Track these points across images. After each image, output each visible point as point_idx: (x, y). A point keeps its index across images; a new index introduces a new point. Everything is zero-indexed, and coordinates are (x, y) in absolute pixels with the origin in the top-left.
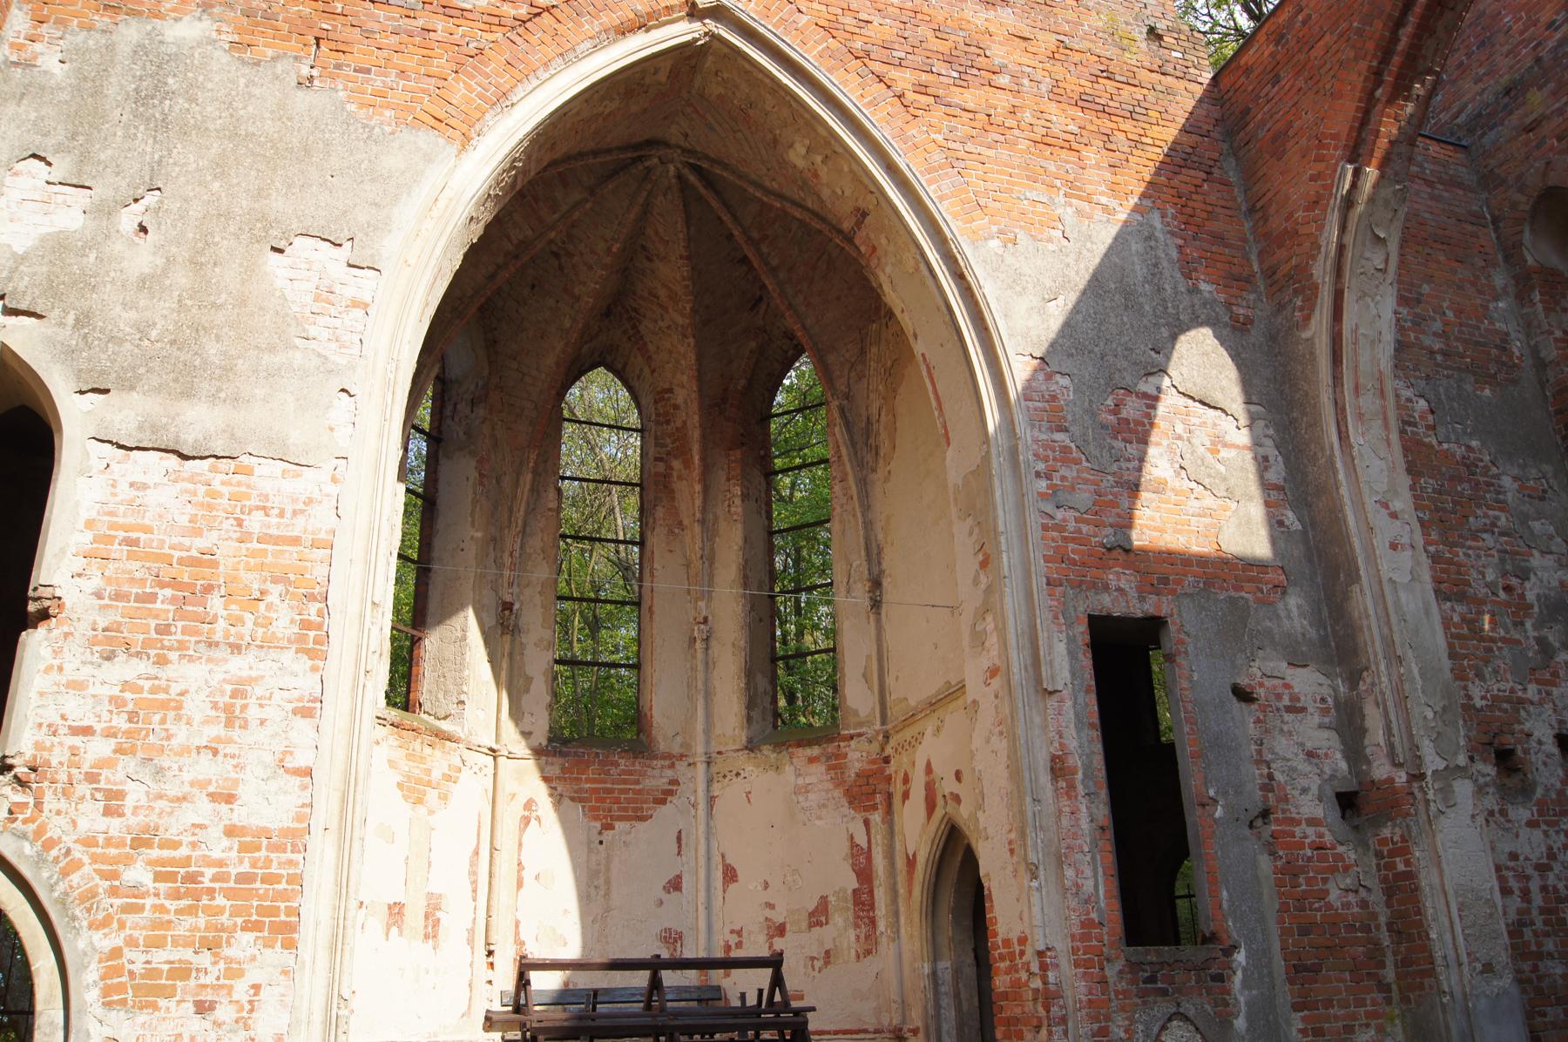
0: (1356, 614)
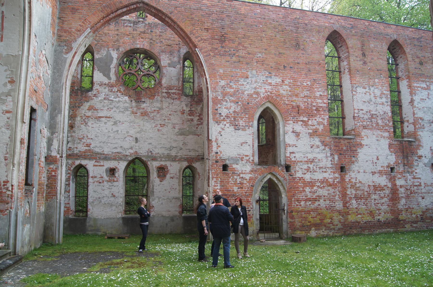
0: (58, 120)
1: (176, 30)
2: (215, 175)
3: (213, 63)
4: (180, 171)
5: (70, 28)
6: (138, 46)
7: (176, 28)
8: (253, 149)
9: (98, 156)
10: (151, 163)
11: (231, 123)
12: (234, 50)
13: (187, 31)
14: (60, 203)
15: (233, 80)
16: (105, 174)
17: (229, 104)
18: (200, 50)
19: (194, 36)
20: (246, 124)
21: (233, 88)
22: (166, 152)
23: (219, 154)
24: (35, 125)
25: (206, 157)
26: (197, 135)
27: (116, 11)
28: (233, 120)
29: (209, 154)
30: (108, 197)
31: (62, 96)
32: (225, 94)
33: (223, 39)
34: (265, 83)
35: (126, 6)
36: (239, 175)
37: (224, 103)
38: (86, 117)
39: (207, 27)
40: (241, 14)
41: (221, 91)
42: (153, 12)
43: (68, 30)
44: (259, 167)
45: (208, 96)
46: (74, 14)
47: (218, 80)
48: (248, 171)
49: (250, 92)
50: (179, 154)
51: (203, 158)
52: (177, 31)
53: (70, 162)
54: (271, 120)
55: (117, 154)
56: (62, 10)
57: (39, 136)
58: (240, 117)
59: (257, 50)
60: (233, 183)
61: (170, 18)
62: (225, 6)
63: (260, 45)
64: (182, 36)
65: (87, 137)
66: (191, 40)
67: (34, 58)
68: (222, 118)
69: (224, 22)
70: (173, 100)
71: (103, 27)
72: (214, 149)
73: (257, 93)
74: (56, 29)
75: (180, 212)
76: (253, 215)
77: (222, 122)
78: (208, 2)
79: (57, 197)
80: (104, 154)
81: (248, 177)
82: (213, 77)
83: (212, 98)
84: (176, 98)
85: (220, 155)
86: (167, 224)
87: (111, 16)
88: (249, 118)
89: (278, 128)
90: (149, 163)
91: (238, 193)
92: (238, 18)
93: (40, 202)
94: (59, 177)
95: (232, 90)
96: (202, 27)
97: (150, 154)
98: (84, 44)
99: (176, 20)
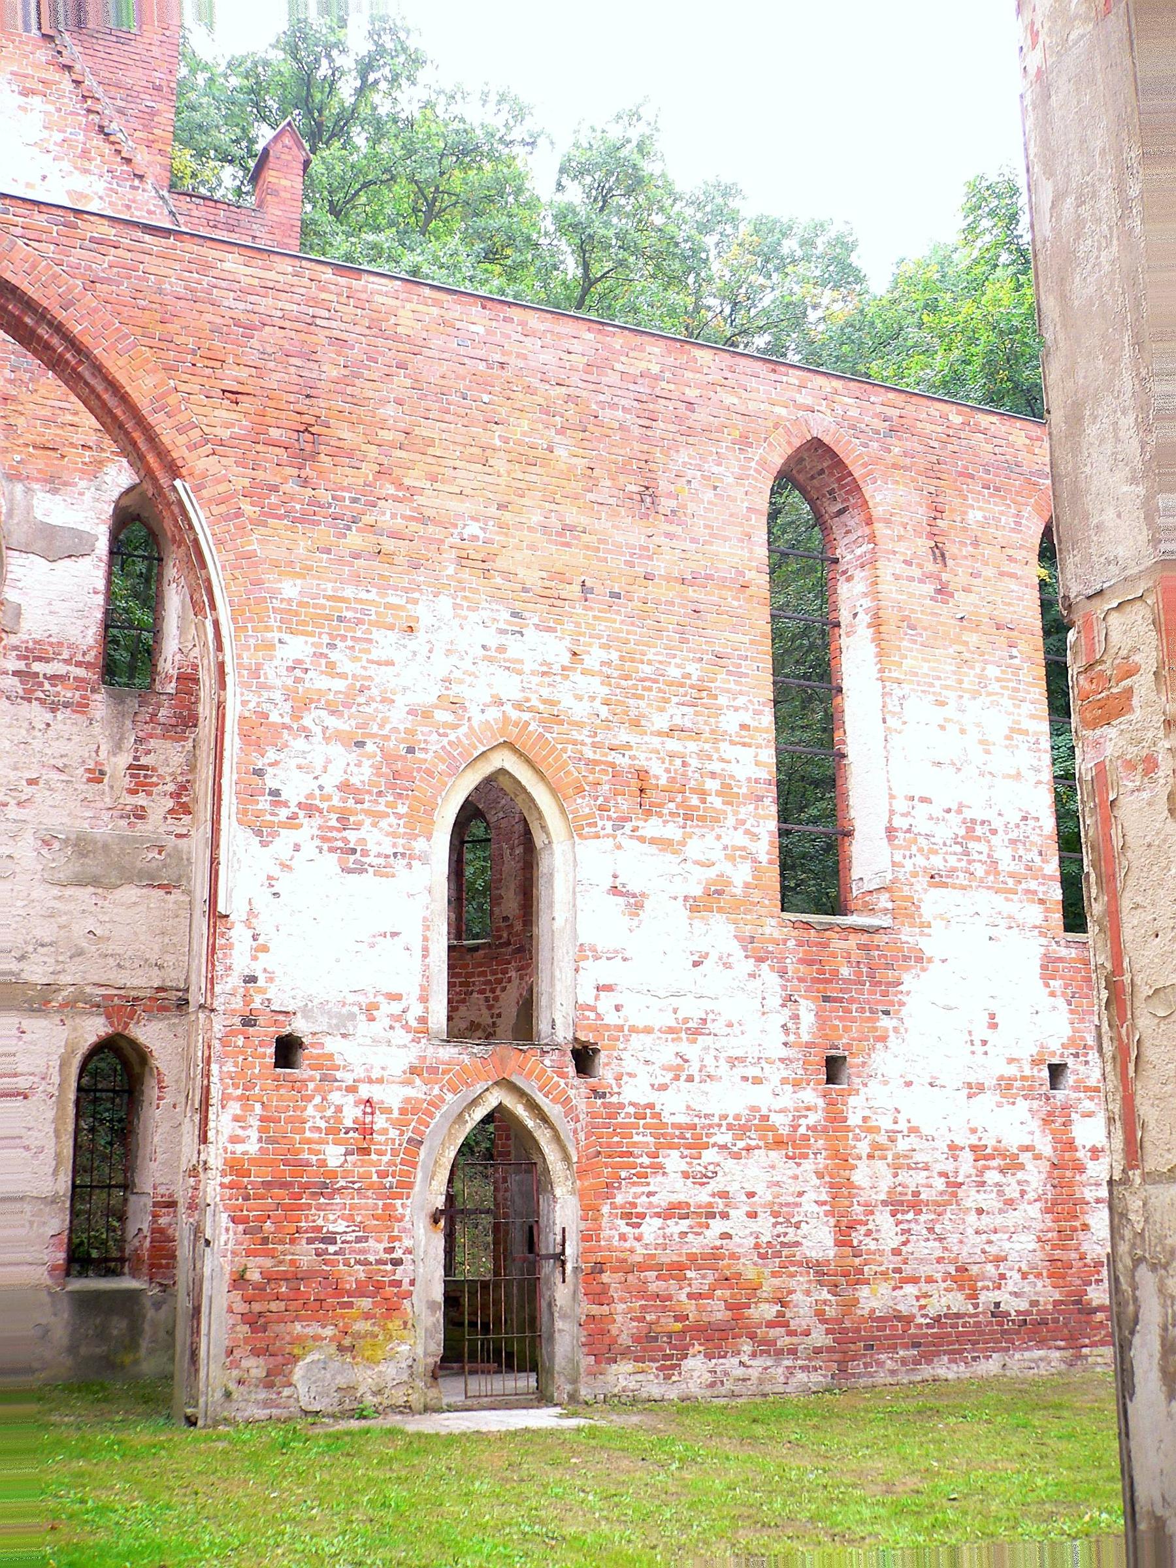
1: (87, 384)
7: (87, 375)
15: (344, 638)
17: (318, 751)
18: (197, 489)
19: (170, 422)
21: (343, 676)
23: (261, 982)
25: (196, 997)
26: (159, 886)
28: (334, 823)
32: (302, 704)
33: (308, 447)
34: (490, 660)
36: (352, 1089)
37: (299, 744)
40: (396, 338)
41: (285, 687)
44: (449, 1052)
45: (221, 706)
50: (65, 979)
51: (182, 1004)
52: (93, 390)
54: (519, 828)
58: (368, 812)
60: (323, 1125)
61: (58, 328)
62: (324, 296)
63: (476, 485)
64: (115, 418)
66: (152, 438)
68: (283, 813)
69: (315, 366)
70: (53, 710)
72: (240, 958)
73: (456, 705)
75: (54, 1268)
78: (249, 271)
81: (392, 1096)
82: (251, 620)
83: (242, 718)
85: (262, 991)
95: (339, 685)
96: (213, 382)
99: (87, 340)
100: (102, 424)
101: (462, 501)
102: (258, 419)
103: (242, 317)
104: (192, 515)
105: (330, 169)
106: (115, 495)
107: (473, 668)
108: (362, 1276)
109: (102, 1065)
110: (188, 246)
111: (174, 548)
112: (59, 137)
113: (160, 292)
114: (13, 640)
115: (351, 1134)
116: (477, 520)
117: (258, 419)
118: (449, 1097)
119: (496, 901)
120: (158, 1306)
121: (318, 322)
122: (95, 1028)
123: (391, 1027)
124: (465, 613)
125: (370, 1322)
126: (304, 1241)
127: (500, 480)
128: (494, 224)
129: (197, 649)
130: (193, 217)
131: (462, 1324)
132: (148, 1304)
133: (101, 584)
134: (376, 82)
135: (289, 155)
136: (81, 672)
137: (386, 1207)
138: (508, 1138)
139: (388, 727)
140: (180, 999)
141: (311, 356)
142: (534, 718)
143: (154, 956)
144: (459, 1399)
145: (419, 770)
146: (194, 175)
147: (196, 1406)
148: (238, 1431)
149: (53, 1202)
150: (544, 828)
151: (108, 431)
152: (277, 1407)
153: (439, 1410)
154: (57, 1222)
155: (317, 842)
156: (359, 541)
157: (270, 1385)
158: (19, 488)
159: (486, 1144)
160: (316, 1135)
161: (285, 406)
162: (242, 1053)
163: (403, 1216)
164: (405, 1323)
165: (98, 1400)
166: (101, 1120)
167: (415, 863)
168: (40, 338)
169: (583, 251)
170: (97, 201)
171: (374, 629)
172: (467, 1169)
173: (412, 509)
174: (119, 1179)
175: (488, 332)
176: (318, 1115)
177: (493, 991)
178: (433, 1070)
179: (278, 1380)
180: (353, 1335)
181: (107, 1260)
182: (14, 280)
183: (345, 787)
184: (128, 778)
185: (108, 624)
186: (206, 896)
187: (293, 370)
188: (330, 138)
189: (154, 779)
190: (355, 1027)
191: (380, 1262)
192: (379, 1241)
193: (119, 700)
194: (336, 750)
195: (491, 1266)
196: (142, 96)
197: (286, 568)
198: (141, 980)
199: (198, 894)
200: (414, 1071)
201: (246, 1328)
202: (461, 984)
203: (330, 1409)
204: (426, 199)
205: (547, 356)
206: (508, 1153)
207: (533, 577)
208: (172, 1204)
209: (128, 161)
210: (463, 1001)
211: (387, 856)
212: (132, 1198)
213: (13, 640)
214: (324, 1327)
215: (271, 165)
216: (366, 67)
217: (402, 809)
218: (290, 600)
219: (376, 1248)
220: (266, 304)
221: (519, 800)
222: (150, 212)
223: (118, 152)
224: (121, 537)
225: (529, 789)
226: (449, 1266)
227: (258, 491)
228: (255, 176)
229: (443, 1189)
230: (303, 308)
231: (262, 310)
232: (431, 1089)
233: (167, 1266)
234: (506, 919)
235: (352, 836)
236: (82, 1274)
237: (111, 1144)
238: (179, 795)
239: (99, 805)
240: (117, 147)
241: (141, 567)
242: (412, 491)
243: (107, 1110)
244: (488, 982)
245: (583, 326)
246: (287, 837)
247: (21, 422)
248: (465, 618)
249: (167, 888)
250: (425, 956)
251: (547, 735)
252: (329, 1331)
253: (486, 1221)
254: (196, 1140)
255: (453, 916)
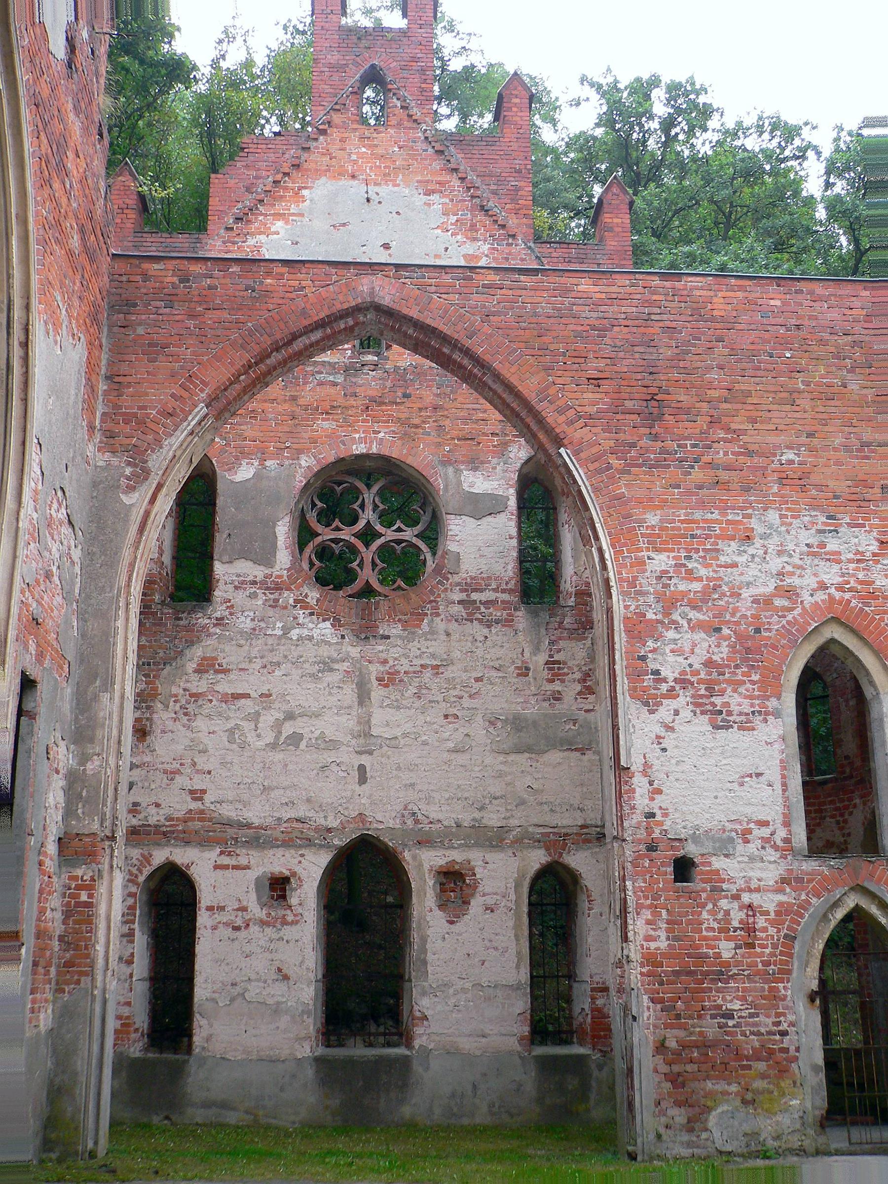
0: (102, 714)
1: (490, 388)
2: (647, 898)
3: (623, 495)
4: (518, 885)
5: (140, 408)
6: (359, 449)
7: (490, 382)
8: (786, 799)
9: (231, 832)
10: (414, 857)
11: (698, 705)
12: (694, 446)
13: (525, 392)
14: (105, 1002)
15: (697, 551)
16: (253, 896)
17: (686, 638)
18: (576, 453)
19: (552, 407)
20: (752, 705)
21: (700, 579)
22: (466, 818)
23: (659, 818)
24: (31, 733)
25: (610, 831)
26: (576, 750)
27: (290, 343)
28: (703, 692)
29: (621, 819)
30: (265, 982)
31: (116, 634)
32: (669, 603)
33: (655, 411)
34: (814, 554)
35: (321, 324)
36: (736, 897)
37: (671, 634)
38: (191, 695)
39: (596, 374)
40: (713, 319)
41: (656, 592)
42: (411, 337)
43: (135, 415)
44: (810, 865)
45: (609, 611)
46: (154, 360)
47: (645, 553)
48: (771, 883)
49: (762, 590)
50: (514, 822)
51: (601, 837)
52: (495, 392)
53: (135, 853)
54: (851, 685)
55: (295, 825)
56: (119, 351)
57: (44, 767)
58: (729, 682)
59: (782, 439)
60: (716, 926)
61: (467, 352)
62: (655, 297)
63: (788, 421)
64: (513, 410)
65: (194, 764)
66: (541, 421)
67: (35, 516)
68: (664, 687)
69: (654, 350)
70: (489, 627)
71: (246, 398)
72: (641, 799)
73: (790, 593)
74: (98, 415)
75: (522, 1038)
76: (798, 1050)
77: (665, 702)
78: (597, 289)
79: (93, 980)
80: (249, 826)
81: (769, 902)
82: (626, 545)
83: (626, 619)
84: (497, 622)
85: (661, 824)
86: (475, 1087)
87: (271, 361)
88: (763, 684)
89: (874, 714)
90: (407, 855)
91: (738, 964)
92: (704, 333)
93: (38, 996)
94: (102, 909)
95: (697, 586)
96: (580, 374)
97: (410, 822)
98: (185, 457)
99: (488, 357)
100: (504, 416)
101: (777, 435)
102: (616, 396)
103: (596, 323)
104: (575, 473)
105: (649, 204)
106: (519, 465)
107: (800, 563)
108: (757, 1044)
109: (545, 886)
110: (552, 279)
111: (564, 498)
112: (453, 219)
113: (536, 314)
114: (456, 579)
115: (739, 932)
116: (791, 448)
117: (616, 396)
118: (814, 901)
119: (838, 743)
120: (600, 1067)
121: (653, 317)
122: (538, 858)
123: (763, 848)
124: (789, 520)
125: (766, 1081)
126: (708, 1017)
127: (806, 415)
128: (779, 223)
129: (587, 571)
130: (554, 257)
131: (841, 1084)
132: (593, 1066)
133: (514, 532)
134: (677, 134)
135: (618, 200)
136: (505, 597)
137: (771, 989)
138: (865, 933)
139: (738, 615)
140: (598, 833)
141: (650, 343)
142: (854, 597)
143: (576, 802)
144: (844, 1145)
145: (766, 645)
146: (550, 228)
147: (635, 1145)
148: (669, 1165)
149: (518, 989)
150: (872, 683)
151: (509, 420)
152: (698, 1147)
153: (829, 1154)
154: (521, 1004)
155: (691, 707)
156: (701, 476)
157: (691, 1130)
158: (450, 470)
159: (847, 940)
160: (711, 934)
161: (635, 383)
162: (649, 872)
163: (786, 996)
164: (795, 1083)
165: (562, 1139)
166: (548, 927)
167: (768, 718)
168: (455, 361)
169: (852, 231)
170: (485, 258)
171: (720, 542)
172: (834, 960)
173: (740, 447)
174: (564, 971)
175: (784, 303)
176: (711, 918)
177: (842, 815)
178: (799, 880)
179: (697, 1126)
180: (753, 1091)
181: (560, 1032)
182: (433, 324)
183: (709, 664)
184: (546, 671)
185: (523, 558)
186: (611, 754)
187: (637, 356)
188: (646, 184)
189: (566, 670)
190: (734, 849)
191: (770, 1033)
192: (768, 1016)
193: (535, 614)
194: (700, 636)
195: (860, 1038)
196: (508, 179)
197: (648, 503)
198: (567, 821)
199: (605, 753)
200: (784, 881)
201: (669, 1085)
202: (816, 811)
203: (739, 1151)
204: (724, 214)
205: (834, 315)
206: (867, 945)
207: (842, 487)
208: (606, 989)
209: (503, 226)
210: (819, 825)
211: (747, 714)
212: (575, 985)
213: (456, 579)
214: (729, 1084)
215: (605, 210)
216: (668, 124)
217: (755, 677)
218: (653, 527)
219: (766, 1022)
220: (612, 310)
221: (849, 662)
222: (522, 260)
223: (496, 221)
224: (526, 496)
225: (856, 654)
226: (827, 1037)
227: (621, 449)
228: (594, 221)
229: (816, 974)
230: (641, 309)
231: (610, 315)
232: (800, 895)
233: (605, 1037)
234: (847, 757)
235: (718, 701)
236: (543, 1043)
237: (556, 945)
238: (585, 681)
239: (528, 692)
240: (495, 218)
241: (541, 516)
242: (738, 432)
243: (551, 920)
244: (836, 809)
245: (859, 286)
246: (670, 705)
247: (447, 423)
248: (791, 524)
249: (582, 751)
250: (784, 791)
251: (867, 609)
252: (734, 1088)
253: (853, 999)
254: (620, 940)
255: (804, 758)
